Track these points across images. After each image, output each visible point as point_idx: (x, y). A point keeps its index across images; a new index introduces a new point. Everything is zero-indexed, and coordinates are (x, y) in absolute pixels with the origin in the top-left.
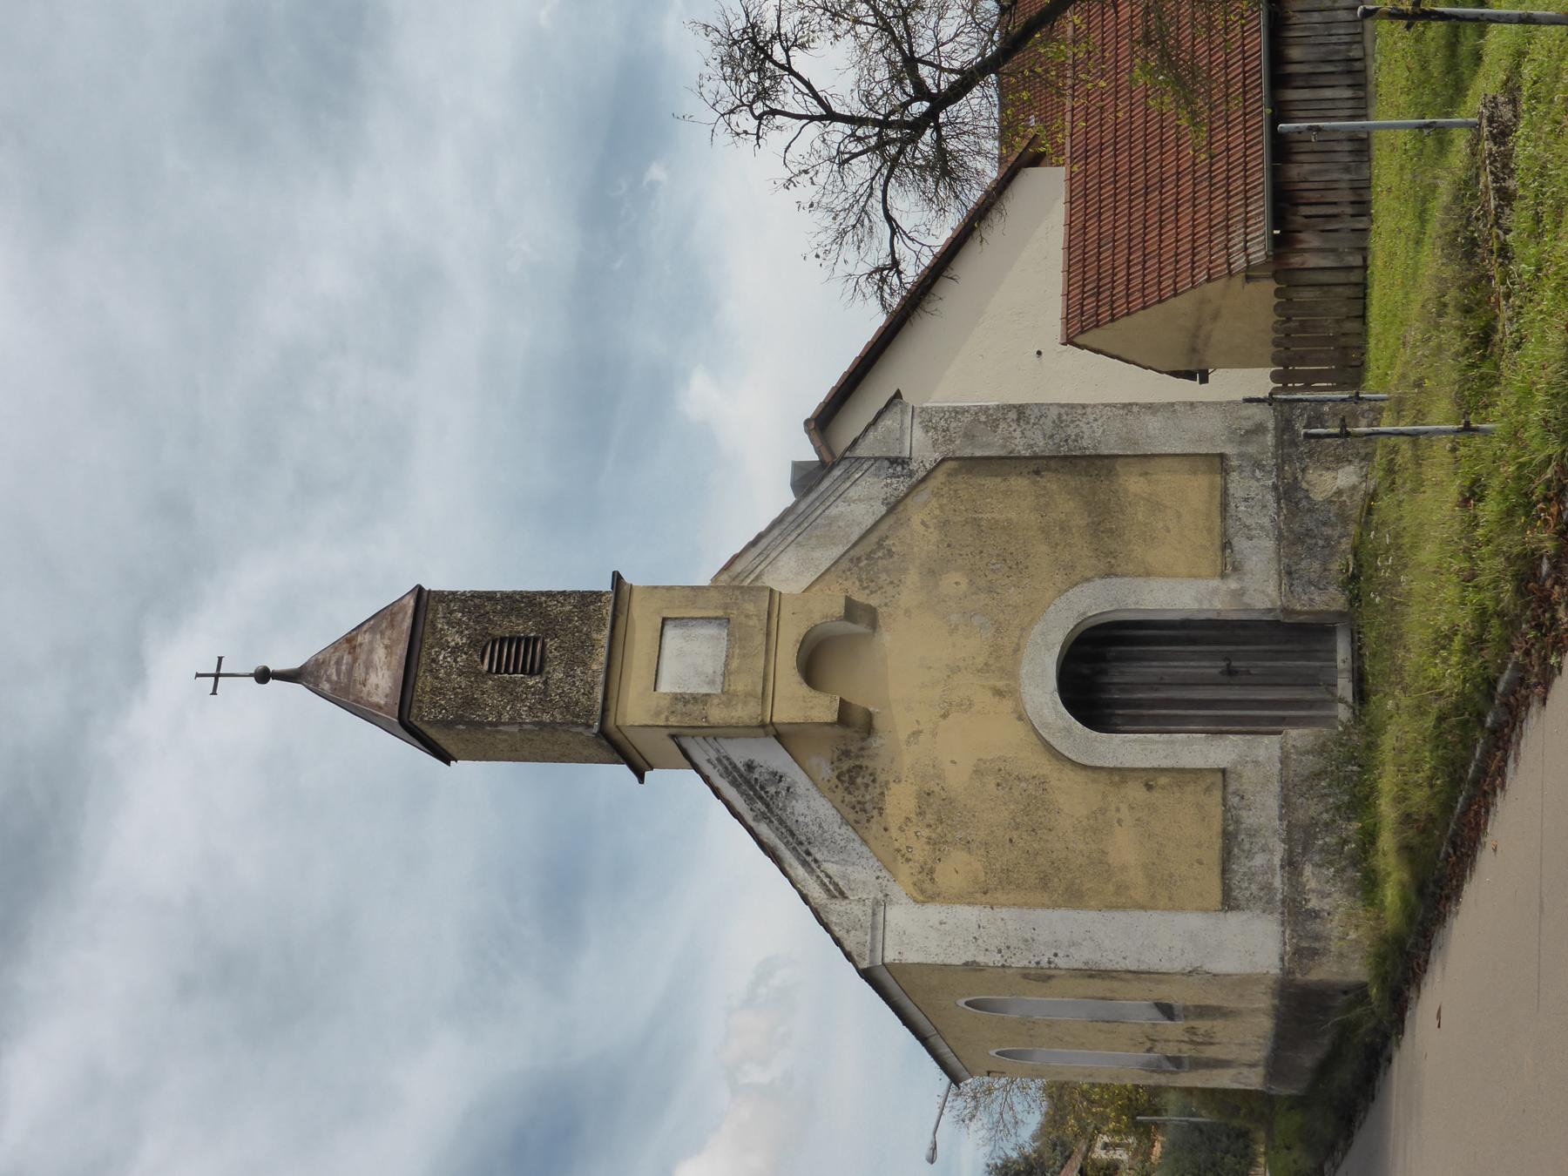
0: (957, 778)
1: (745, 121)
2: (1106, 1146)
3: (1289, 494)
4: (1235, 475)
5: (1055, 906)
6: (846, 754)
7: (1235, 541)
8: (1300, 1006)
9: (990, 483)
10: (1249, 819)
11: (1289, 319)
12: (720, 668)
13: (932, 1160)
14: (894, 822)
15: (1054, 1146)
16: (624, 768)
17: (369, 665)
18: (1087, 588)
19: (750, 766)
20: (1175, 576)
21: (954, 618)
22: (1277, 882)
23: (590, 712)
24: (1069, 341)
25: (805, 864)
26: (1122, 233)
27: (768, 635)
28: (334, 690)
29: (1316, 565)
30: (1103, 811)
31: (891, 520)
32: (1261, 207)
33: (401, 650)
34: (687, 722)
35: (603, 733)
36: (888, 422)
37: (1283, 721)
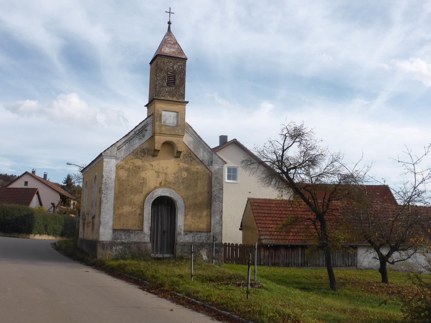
0: (143, 174)
1: (285, 132)
2: (74, 203)
3: (201, 245)
4: (206, 234)
5: (115, 194)
6: (148, 151)
7: (192, 234)
8: (94, 245)
9: (206, 182)
10: (132, 235)
11: (249, 248)
12: (167, 124)
13: (67, 164)
14: (134, 161)
15: (74, 191)
16: (148, 102)
17: (170, 48)
18: (183, 202)
19: (146, 130)
20: (185, 221)
21: (177, 174)
22: (119, 241)
23: (158, 96)
24: (249, 199)
25: (125, 142)
26: (272, 212)
27: (174, 135)
28: (165, 39)
29: (186, 251)
30: (135, 205)
31: (199, 161)
32: (274, 242)
33: (173, 55)
34: (156, 117)
35: (154, 99)
36: (220, 161)
37: (153, 243)
